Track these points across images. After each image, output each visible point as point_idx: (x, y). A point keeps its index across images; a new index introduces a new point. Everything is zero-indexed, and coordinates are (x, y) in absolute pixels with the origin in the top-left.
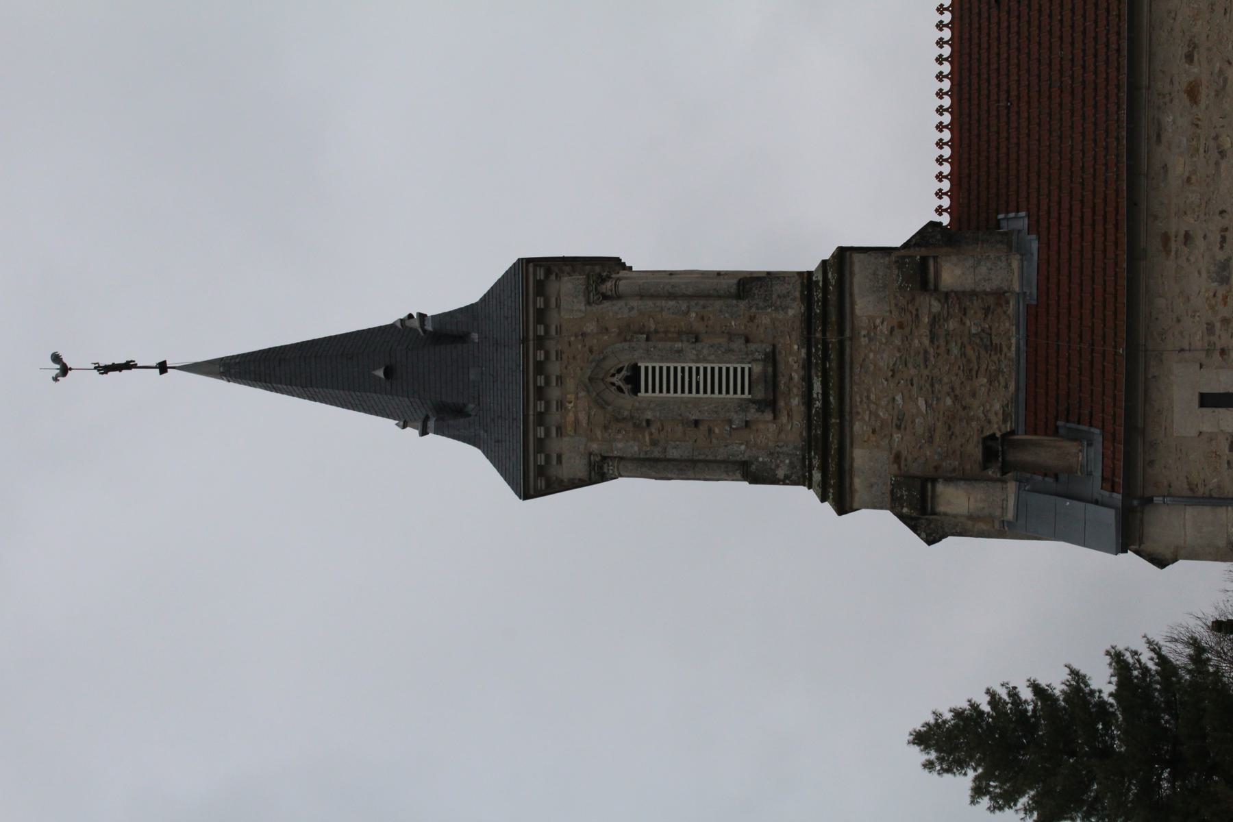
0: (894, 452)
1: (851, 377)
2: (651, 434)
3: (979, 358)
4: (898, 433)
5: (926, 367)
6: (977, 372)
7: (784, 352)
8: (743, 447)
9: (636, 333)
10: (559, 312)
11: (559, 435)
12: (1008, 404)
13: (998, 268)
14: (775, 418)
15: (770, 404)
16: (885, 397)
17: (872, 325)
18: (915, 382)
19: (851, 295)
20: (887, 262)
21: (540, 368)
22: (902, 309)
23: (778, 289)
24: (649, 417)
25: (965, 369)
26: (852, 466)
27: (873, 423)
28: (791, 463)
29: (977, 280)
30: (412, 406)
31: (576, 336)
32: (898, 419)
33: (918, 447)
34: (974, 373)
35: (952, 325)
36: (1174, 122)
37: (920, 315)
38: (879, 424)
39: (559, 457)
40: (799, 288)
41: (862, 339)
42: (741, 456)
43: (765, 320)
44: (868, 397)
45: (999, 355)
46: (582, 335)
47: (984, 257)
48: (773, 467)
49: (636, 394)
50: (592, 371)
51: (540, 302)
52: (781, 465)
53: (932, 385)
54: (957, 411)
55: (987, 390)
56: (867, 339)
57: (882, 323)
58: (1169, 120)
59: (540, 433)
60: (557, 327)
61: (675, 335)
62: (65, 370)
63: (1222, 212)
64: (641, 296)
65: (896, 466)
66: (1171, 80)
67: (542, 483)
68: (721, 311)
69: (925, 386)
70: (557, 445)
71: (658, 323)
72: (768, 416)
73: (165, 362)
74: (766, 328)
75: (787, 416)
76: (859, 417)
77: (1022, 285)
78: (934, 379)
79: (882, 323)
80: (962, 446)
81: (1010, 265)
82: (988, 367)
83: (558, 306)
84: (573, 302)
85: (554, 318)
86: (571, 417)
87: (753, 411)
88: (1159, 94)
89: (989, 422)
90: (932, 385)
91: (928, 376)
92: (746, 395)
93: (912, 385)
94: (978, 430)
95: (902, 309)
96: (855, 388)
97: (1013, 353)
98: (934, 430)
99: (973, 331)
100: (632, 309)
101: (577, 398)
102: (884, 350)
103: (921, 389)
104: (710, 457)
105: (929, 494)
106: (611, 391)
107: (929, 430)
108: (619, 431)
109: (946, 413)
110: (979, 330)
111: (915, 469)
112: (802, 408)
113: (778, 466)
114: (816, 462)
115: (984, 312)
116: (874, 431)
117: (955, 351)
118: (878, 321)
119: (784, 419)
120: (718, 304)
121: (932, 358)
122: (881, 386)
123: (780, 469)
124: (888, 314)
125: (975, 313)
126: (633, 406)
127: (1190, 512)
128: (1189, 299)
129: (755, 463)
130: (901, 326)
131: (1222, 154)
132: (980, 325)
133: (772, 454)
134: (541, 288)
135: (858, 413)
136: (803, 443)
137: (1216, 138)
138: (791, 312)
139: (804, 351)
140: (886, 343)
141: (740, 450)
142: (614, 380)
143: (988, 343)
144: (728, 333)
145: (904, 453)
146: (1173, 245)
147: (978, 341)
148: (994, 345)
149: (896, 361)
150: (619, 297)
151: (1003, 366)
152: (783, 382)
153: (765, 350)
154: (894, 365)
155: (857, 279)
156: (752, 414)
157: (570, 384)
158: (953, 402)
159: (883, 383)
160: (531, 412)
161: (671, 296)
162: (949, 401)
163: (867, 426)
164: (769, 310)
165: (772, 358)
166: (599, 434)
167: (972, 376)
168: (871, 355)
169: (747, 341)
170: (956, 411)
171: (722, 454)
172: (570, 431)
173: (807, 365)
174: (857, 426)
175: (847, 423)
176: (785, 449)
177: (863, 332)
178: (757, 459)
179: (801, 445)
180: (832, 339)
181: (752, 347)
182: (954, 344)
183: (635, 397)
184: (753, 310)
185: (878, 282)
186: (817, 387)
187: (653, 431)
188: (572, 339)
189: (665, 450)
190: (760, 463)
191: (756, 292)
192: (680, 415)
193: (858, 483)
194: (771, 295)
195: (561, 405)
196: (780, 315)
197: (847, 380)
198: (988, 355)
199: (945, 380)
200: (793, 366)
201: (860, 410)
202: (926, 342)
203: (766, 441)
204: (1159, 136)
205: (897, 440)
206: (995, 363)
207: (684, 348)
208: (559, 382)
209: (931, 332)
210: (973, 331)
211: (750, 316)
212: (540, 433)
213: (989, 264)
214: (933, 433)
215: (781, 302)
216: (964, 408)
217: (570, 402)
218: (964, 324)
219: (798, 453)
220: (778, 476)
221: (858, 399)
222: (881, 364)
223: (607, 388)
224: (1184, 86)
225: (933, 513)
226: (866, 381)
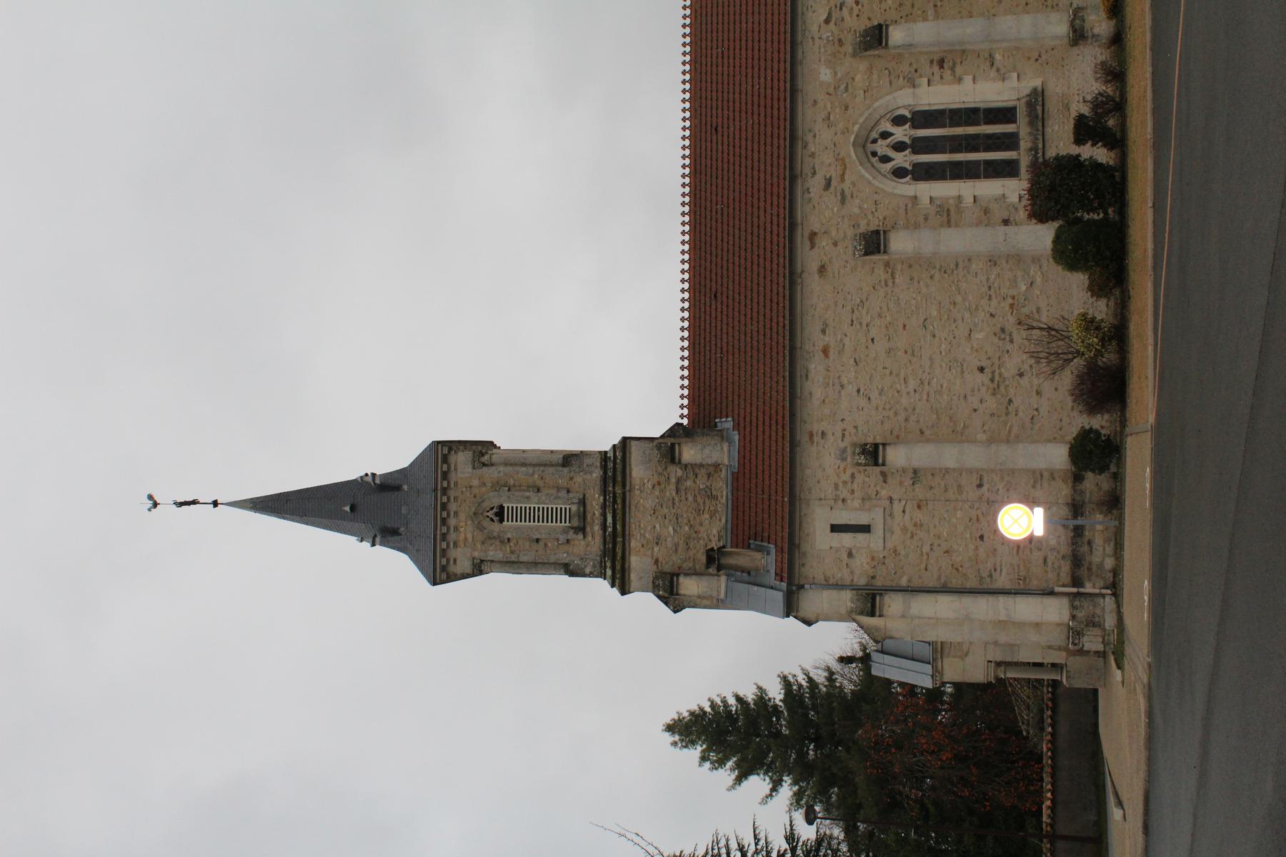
0: (654, 558)
1: (630, 513)
2: (510, 547)
3: (704, 503)
5: (674, 508)
8: (565, 555)
14: (584, 537)
15: (581, 529)
18: (667, 517)
19: (630, 465)
21: (444, 507)
23: (587, 461)
26: (629, 566)
28: (594, 564)
31: (466, 488)
35: (689, 483)
36: (815, 368)
39: (455, 561)
40: (599, 460)
43: (578, 479)
44: (639, 526)
49: (501, 523)
53: (677, 519)
62: (155, 505)
63: (843, 420)
64: (506, 464)
67: (444, 576)
68: (553, 474)
70: (453, 553)
73: (216, 501)
77: (729, 461)
81: (722, 449)
85: (453, 477)
87: (571, 533)
89: (710, 540)
90: (677, 519)
92: (567, 524)
93: (665, 518)
96: (632, 520)
97: (724, 500)
99: (701, 487)
100: (499, 472)
101: (466, 525)
104: (546, 561)
105: (675, 583)
107: (675, 545)
111: (667, 568)
112: (601, 532)
113: (586, 566)
114: (608, 564)
116: (643, 546)
117: (691, 499)
118: (646, 481)
120: (551, 470)
127: (827, 594)
128: (824, 470)
130: (659, 483)
131: (842, 386)
133: (582, 559)
134: (445, 459)
135: (633, 535)
137: (839, 377)
138: (594, 475)
139: (602, 498)
141: (563, 557)
142: (489, 514)
145: (660, 559)
146: (816, 439)
147: (704, 493)
150: (492, 465)
154: (655, 506)
156: (571, 535)
157: (462, 516)
160: (438, 533)
161: (524, 465)
165: (583, 502)
166: (479, 546)
168: (642, 500)
169: (568, 492)
173: (604, 506)
174: (633, 544)
177: (637, 487)
178: (574, 562)
180: (619, 491)
181: (571, 495)
186: (610, 520)
188: (464, 489)
189: (518, 557)
193: (633, 576)
195: (456, 529)
196: (588, 477)
197: (627, 515)
199: (685, 516)
202: (674, 493)
204: (807, 376)
210: (701, 487)
216: (696, 532)
217: (462, 527)
218: (696, 483)
222: (647, 506)
224: (821, 348)
225: (677, 594)
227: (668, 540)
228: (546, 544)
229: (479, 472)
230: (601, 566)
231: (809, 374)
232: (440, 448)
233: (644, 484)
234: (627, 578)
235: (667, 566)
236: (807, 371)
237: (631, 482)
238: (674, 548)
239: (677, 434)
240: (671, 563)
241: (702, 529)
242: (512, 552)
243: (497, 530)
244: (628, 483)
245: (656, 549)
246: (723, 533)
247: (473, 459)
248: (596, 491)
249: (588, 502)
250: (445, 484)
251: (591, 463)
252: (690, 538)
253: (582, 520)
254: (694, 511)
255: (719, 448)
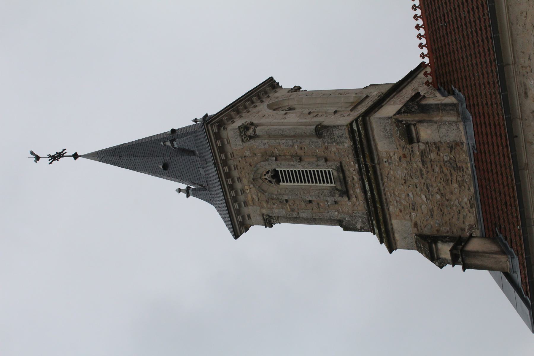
0: (413, 222)
1: (383, 183)
3: (451, 174)
4: (414, 212)
5: (423, 178)
6: (451, 181)
7: (346, 165)
8: (336, 213)
9: (270, 156)
10: (231, 146)
11: (246, 205)
12: (472, 198)
13: (452, 129)
14: (349, 199)
15: (346, 193)
16: (403, 193)
17: (389, 156)
18: (418, 186)
19: (374, 140)
20: (390, 122)
21: (228, 175)
22: (403, 147)
23: (337, 133)
24: (286, 199)
25: (444, 179)
26: (392, 228)
27: (400, 207)
28: (362, 221)
29: (441, 136)
30: (181, 172)
31: (241, 158)
32: (413, 205)
33: (426, 219)
34: (450, 182)
35: (433, 156)
37: (414, 151)
38: (403, 207)
39: (249, 216)
41: (385, 164)
42: (336, 217)
44: (394, 194)
45: (462, 172)
46: (244, 157)
47: (443, 124)
48: (354, 223)
49: (279, 184)
50: (253, 176)
51: (219, 143)
52: (358, 222)
53: (428, 188)
54: (444, 201)
55: (459, 191)
56: (387, 163)
57: (394, 155)
58: (531, 83)
59: (236, 207)
60: (231, 154)
61: (289, 157)
65: (416, 229)
66: (529, 57)
68: (309, 144)
69: (424, 188)
71: (280, 151)
72: (346, 199)
74: (335, 153)
75: (355, 198)
76: (392, 204)
78: (428, 185)
79: (394, 155)
80: (449, 220)
81: (458, 128)
82: (457, 178)
83: (229, 143)
84: (236, 141)
85: (228, 149)
86: (249, 197)
87: (337, 195)
88: (522, 67)
89: (463, 208)
90: (428, 188)
91: (424, 183)
93: (417, 188)
94: (457, 212)
95: (403, 147)
96: (386, 189)
97: (470, 171)
98: (433, 212)
99: (445, 159)
100: (265, 144)
102: (398, 169)
103: (422, 190)
105: (435, 250)
106: (266, 183)
107: (430, 211)
108: (274, 204)
109: (438, 203)
110: (449, 159)
111: (427, 231)
112: (363, 194)
113: (356, 223)
115: (449, 149)
116: (401, 211)
117: (437, 170)
118: (392, 154)
119: (354, 199)
120: (307, 141)
121: (425, 174)
122: (400, 188)
123: (357, 224)
124: (396, 150)
125: (445, 149)
126: (278, 192)
129: (344, 221)
130: (405, 156)
132: (449, 156)
133: (352, 216)
135: (390, 202)
136: (367, 212)
138: (346, 145)
139: (357, 165)
140: (398, 165)
142: (266, 177)
143: (455, 166)
144: (316, 156)
145: (419, 223)
147: (449, 165)
148: (458, 167)
149: (405, 175)
151: (466, 178)
152: (349, 181)
153: (336, 165)
154: (405, 176)
155: (375, 132)
156: (337, 198)
157: (245, 181)
158: (441, 197)
159: (400, 186)
161: (284, 136)
162: (438, 197)
163: (396, 208)
164: (334, 144)
165: (341, 169)
166: (265, 205)
167: (449, 183)
168: (392, 172)
169: (326, 160)
170: (443, 201)
171: (327, 216)
172: (251, 203)
174: (391, 208)
175: (385, 207)
176: (358, 214)
177: (385, 160)
178: (345, 219)
179: (366, 213)
180: (370, 164)
182: (436, 166)
183: (278, 186)
184: (326, 144)
185: (387, 133)
187: (290, 204)
188: (240, 159)
189: (298, 214)
190: (347, 221)
191: (325, 134)
192: (301, 198)
193: (397, 236)
194: (334, 136)
195: (243, 191)
196: (341, 147)
197: (381, 185)
198: (456, 172)
199: (434, 185)
200: (353, 173)
201: (391, 200)
202: (420, 165)
203: (348, 210)
204: (526, 93)
205: (414, 216)
206: (461, 177)
207: (295, 165)
208: (239, 180)
209: (422, 159)
210: (445, 159)
211: (325, 147)
212: (236, 207)
213: (446, 127)
214: (432, 213)
215: (340, 140)
216: (448, 200)
217: (248, 190)
218: (439, 155)
219: (365, 216)
220: (357, 227)
221: (389, 195)
222: (398, 176)
223: (264, 182)
226: (391, 185)
227: (423, 206)
228: (318, 204)
229: (248, 144)
230: (369, 223)
231: (528, 91)
232: (210, 128)
233: (391, 157)
234: (392, 238)
235: (426, 229)
236: (526, 89)
237: (378, 155)
238: (429, 213)
239: (413, 110)
240: (429, 227)
241: (454, 198)
242: (293, 210)
243: (275, 193)
244: (376, 157)
245: (413, 214)
246: (473, 201)
247: (240, 134)
248: (350, 159)
249: (346, 168)
250: (223, 157)
251: (340, 134)
252: (442, 205)
253: (344, 186)
254: (442, 181)
255: (455, 127)
